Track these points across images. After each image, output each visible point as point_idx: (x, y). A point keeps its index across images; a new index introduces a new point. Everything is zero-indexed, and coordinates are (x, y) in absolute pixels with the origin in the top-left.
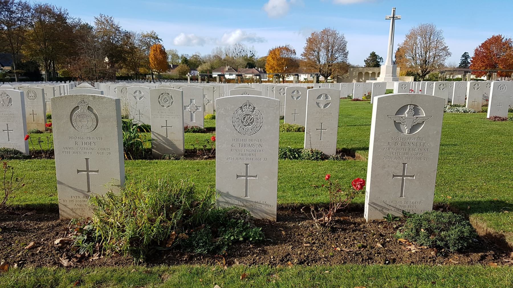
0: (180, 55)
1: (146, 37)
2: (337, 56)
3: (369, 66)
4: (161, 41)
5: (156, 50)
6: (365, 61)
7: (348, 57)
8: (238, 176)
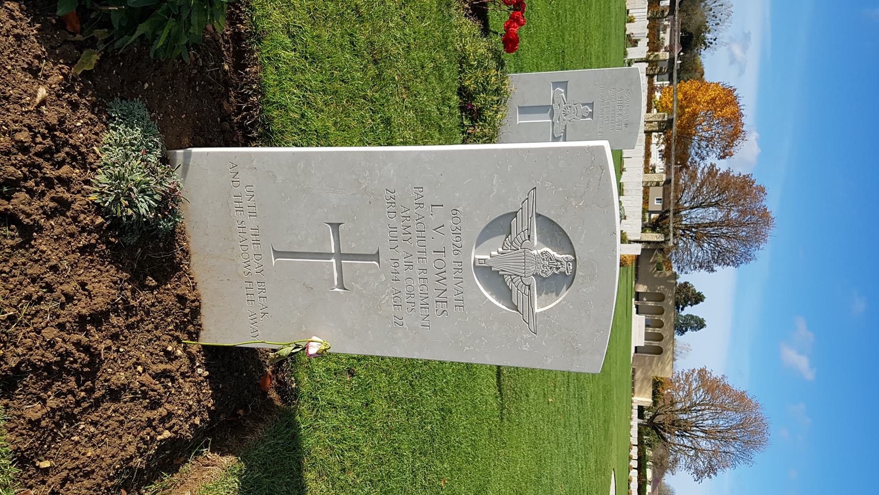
8: (336, 226)
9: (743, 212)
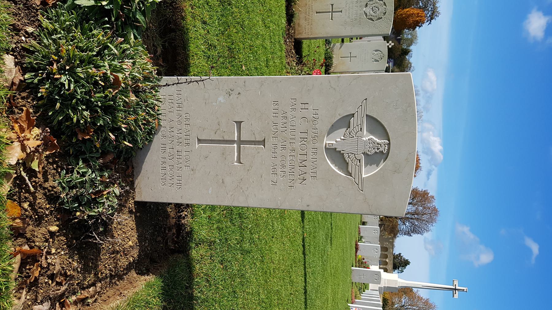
0: (411, 48)
1: (434, 6)
2: (407, 224)
3: (394, 258)
4: (428, 23)
5: (418, 16)
6: (400, 254)
7: (405, 236)
9: (424, 208)
